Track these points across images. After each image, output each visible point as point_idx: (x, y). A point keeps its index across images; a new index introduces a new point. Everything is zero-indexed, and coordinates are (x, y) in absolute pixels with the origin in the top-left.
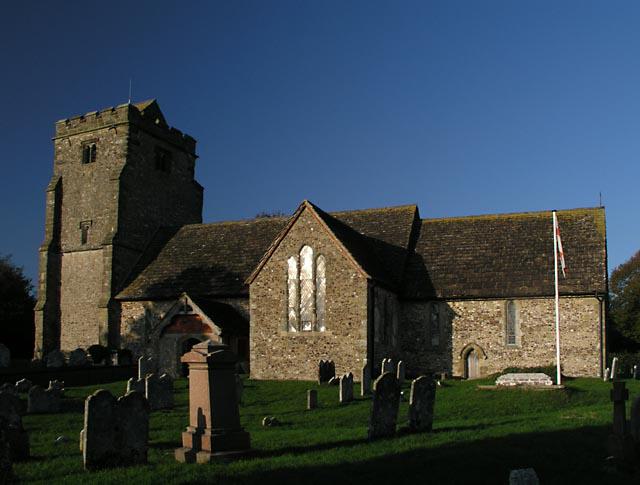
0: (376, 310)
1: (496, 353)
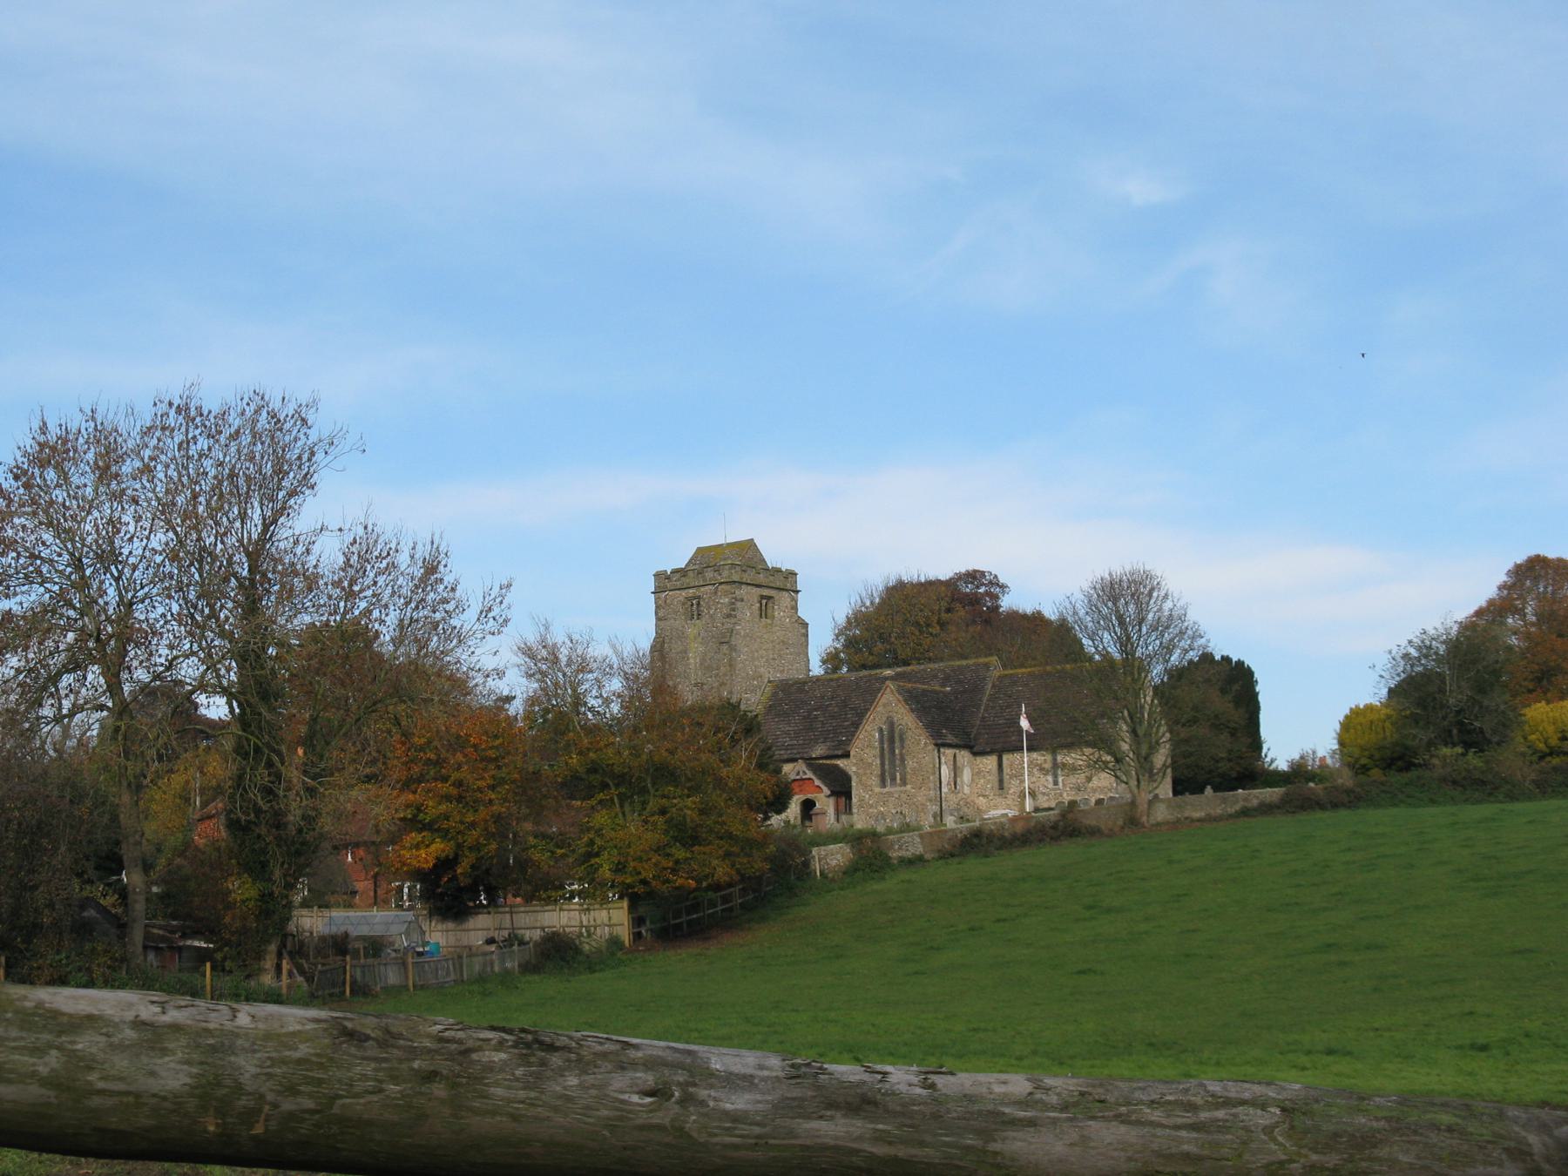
0: (944, 767)
1: (1044, 794)
